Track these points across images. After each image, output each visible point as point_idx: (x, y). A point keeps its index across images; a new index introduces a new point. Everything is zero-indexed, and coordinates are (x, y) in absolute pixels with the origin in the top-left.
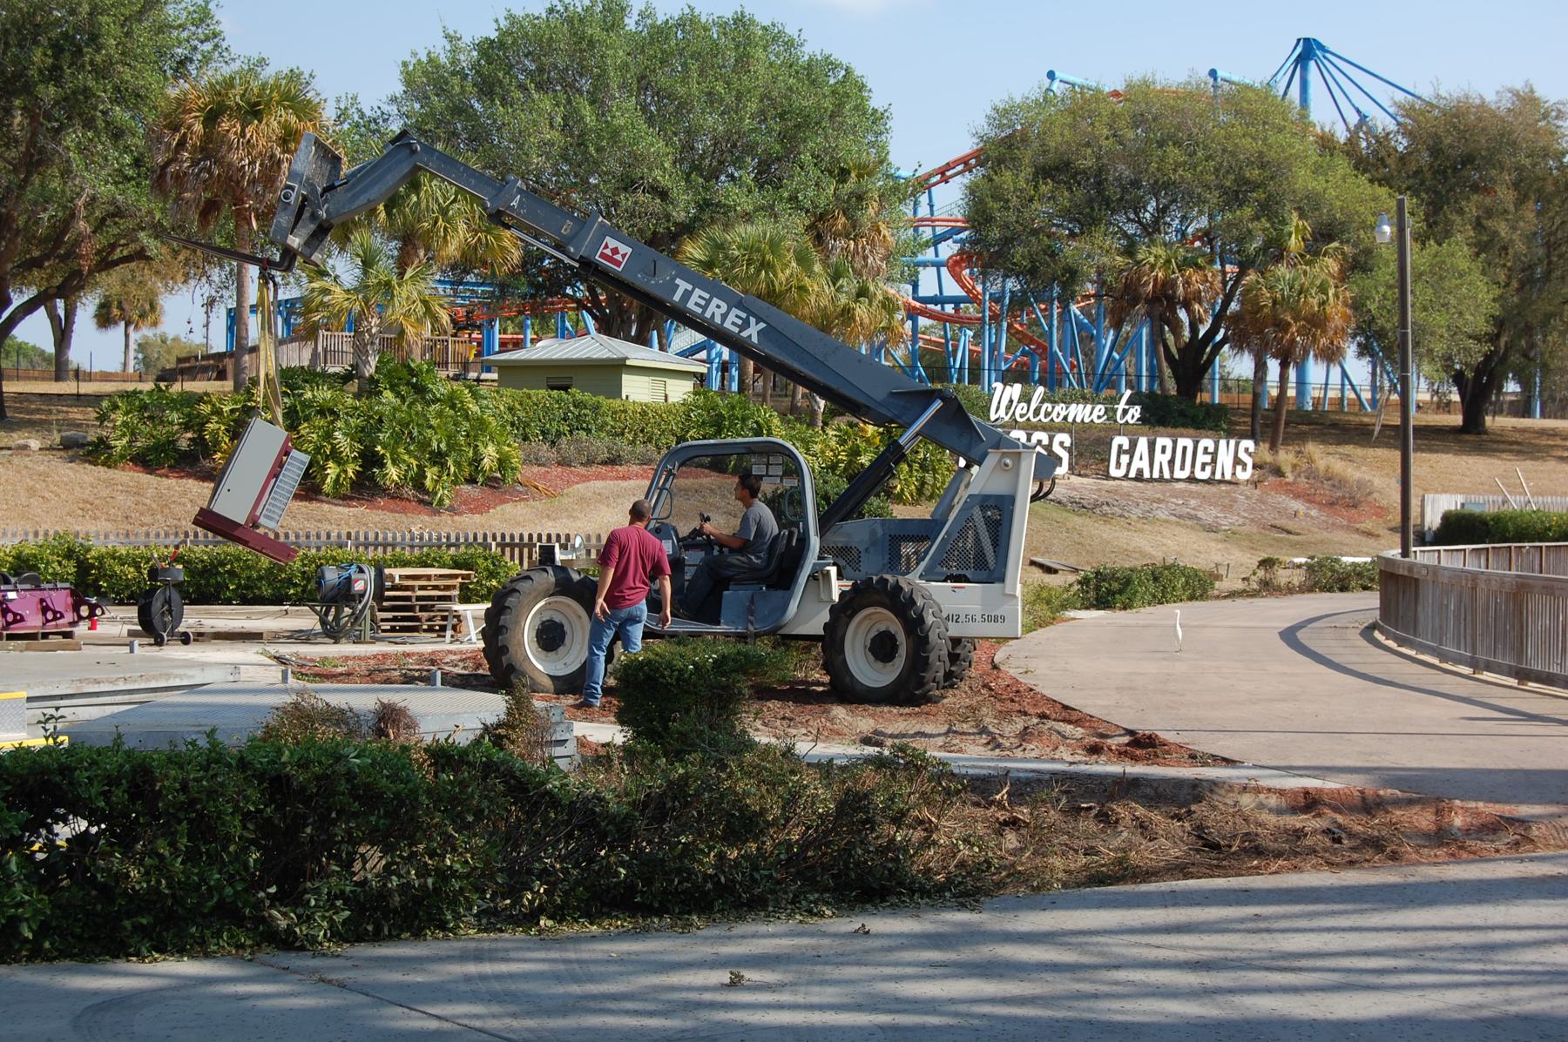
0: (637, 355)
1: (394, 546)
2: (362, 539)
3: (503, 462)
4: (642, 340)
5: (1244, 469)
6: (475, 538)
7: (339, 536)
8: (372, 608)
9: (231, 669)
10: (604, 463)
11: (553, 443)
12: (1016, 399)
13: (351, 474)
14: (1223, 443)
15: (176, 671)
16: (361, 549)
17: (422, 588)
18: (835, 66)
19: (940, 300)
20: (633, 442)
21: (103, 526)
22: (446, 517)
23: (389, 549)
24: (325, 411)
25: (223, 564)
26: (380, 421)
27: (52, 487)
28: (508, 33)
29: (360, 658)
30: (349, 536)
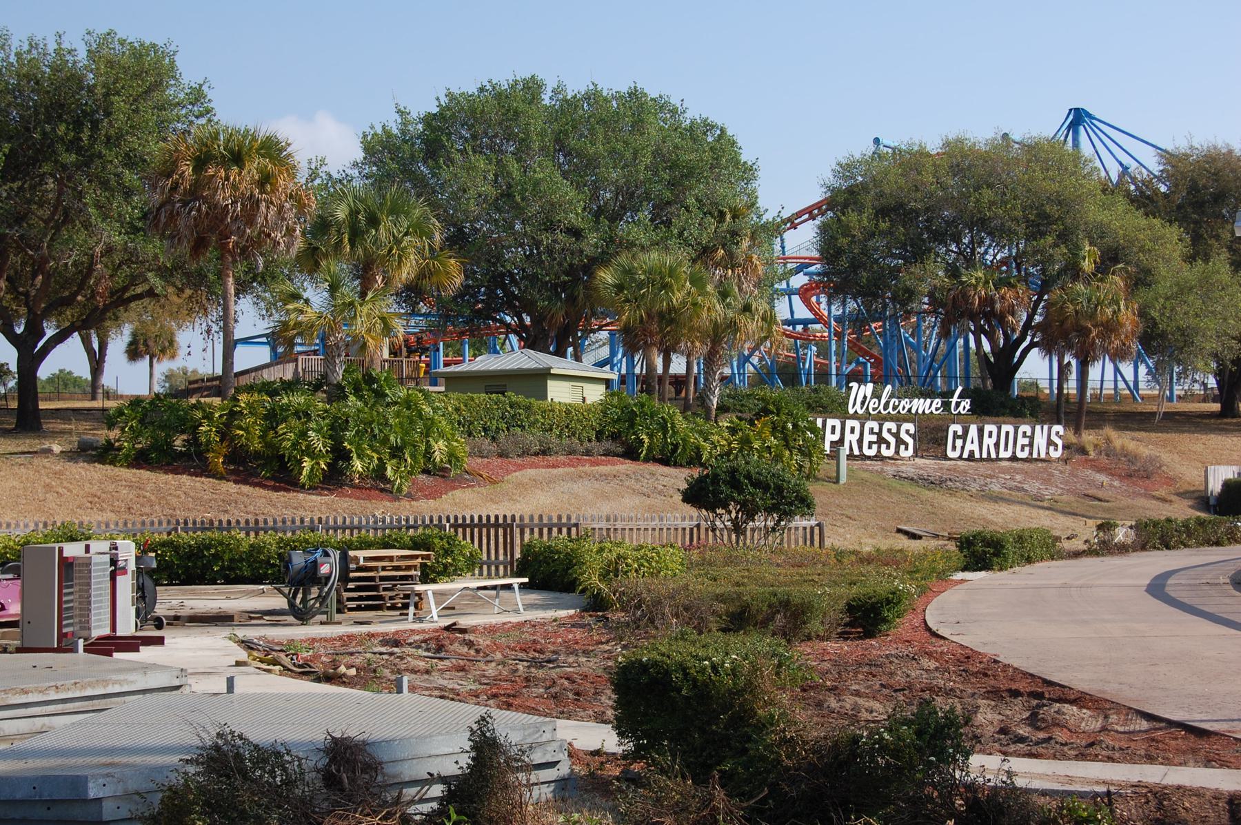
0: (560, 366)
1: (352, 529)
2: (331, 523)
3: (452, 456)
4: (560, 353)
5: (1056, 450)
6: (431, 520)
7: (312, 520)
8: (338, 591)
10: (536, 454)
11: (493, 438)
12: (869, 395)
14: (1038, 428)
15: (114, 677)
17: (384, 569)
19: (792, 322)
20: (560, 436)
21: (109, 516)
22: (405, 503)
23: (356, 531)
24: (303, 414)
26: (347, 421)
27: (65, 484)
28: (448, 108)
29: (326, 640)
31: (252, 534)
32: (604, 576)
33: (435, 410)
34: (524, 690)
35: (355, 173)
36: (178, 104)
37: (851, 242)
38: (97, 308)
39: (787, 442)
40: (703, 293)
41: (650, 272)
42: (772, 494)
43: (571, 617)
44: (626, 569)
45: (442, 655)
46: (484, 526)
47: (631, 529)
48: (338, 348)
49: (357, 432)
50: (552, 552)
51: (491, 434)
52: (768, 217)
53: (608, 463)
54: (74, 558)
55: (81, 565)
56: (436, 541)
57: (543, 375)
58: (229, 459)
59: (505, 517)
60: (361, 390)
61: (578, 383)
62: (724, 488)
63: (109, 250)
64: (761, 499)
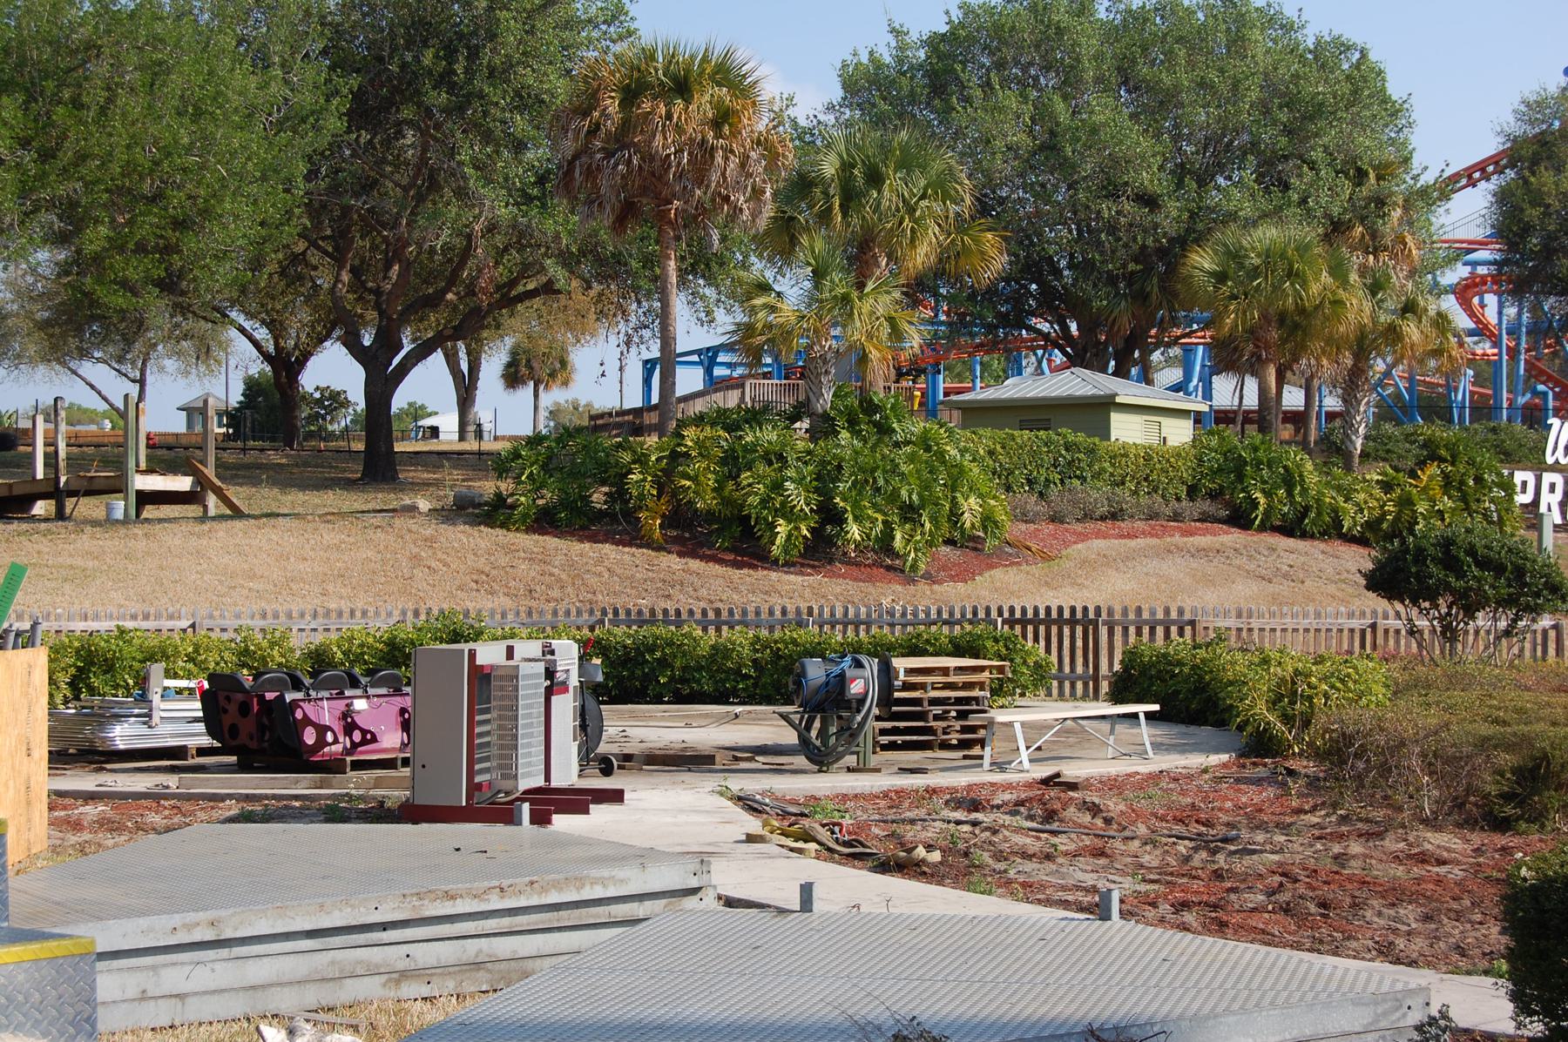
0: (1128, 391)
1: (857, 624)
2: (826, 615)
3: (988, 520)
4: (1121, 372)
9: (693, 865)
10: (1103, 518)
11: (1041, 494)
13: (805, 532)
15: (595, 873)
16: (826, 628)
18: (1347, 48)
20: (1135, 493)
21: (504, 602)
22: (923, 587)
24: (776, 457)
25: (652, 650)
26: (839, 467)
30: (810, 611)
31: (712, 630)
32: (1273, 704)
33: (962, 452)
34: (1233, 897)
35: (830, 119)
36: (590, 21)
37: (1544, 214)
38: (479, 309)
39: (1467, 503)
40: (1344, 283)
41: (1267, 254)
42: (1508, 579)
43: (1225, 765)
44: (1308, 692)
45: (1055, 826)
46: (1055, 622)
47: (1273, 630)
48: (825, 362)
49: (855, 483)
50: (1170, 663)
51: (1038, 488)
52: (1428, 178)
53: (1205, 532)
54: (492, 667)
55: (501, 678)
56: (989, 644)
57: (1107, 404)
58: (670, 521)
59: (1085, 609)
60: (858, 424)
61: (1155, 416)
62: (1433, 569)
63: (492, 228)
64: (1493, 587)
